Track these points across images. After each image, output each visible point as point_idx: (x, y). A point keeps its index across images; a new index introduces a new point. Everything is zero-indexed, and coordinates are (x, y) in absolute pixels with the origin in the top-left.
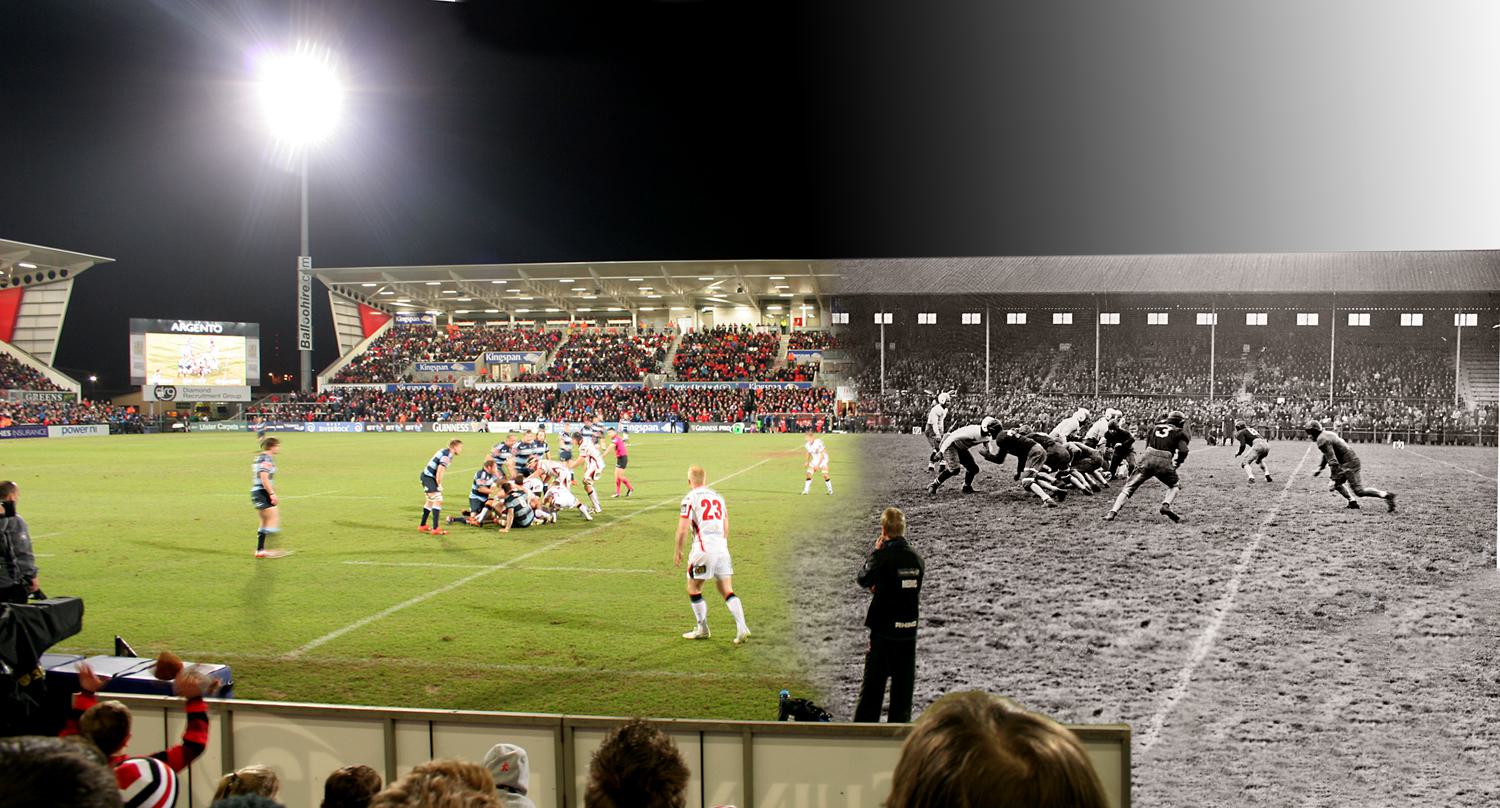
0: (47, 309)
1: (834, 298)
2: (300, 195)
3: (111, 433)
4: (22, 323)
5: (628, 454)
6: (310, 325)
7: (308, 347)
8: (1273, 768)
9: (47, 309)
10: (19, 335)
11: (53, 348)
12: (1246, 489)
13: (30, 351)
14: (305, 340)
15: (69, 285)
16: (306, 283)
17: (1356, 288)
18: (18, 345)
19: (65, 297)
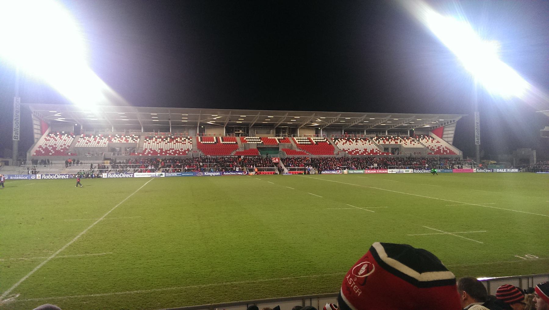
0: (450, 132)
1: (174, 160)
2: (322, 131)
3: (388, 148)
4: (445, 133)
5: (546, 281)
6: (479, 136)
7: (479, 143)
8: (190, 268)
9: (450, 132)
10: (444, 136)
11: (451, 139)
12: (62, 261)
13: (446, 140)
14: (477, 141)
15: (455, 125)
16: (478, 121)
17: (38, 142)
18: (443, 139)
19: (454, 128)
